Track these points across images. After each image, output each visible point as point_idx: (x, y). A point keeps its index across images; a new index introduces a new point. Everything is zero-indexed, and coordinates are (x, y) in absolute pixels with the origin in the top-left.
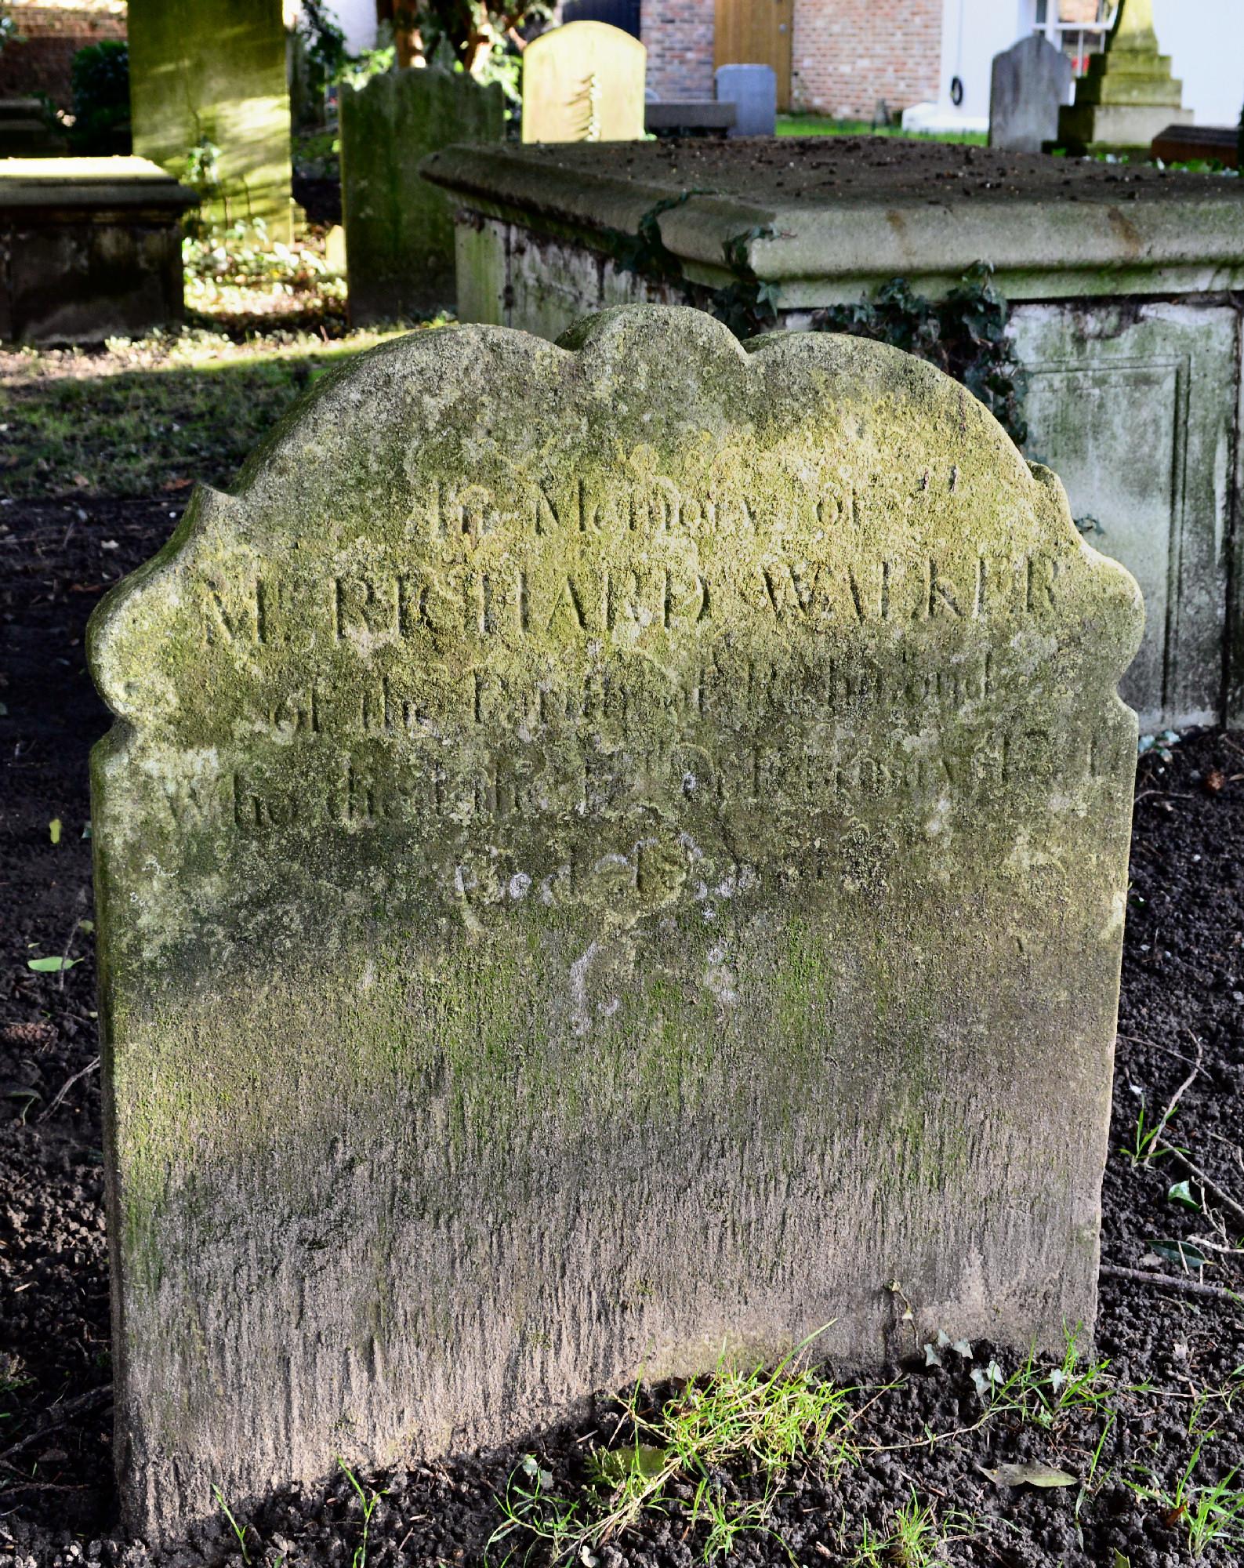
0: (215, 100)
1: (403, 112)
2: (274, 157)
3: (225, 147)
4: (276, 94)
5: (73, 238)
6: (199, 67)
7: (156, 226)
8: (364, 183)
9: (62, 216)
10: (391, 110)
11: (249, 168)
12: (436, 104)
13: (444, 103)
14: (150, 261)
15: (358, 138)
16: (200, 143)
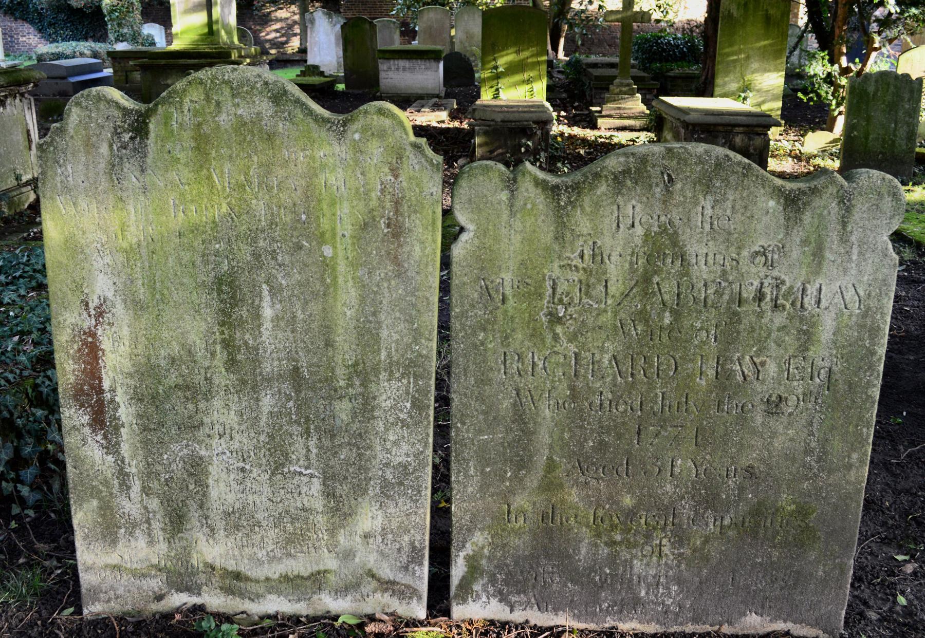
0: (753, 73)
1: (877, 90)
2: (775, 98)
3: (754, 93)
4: (780, 71)
5: (724, 138)
6: (748, 58)
7: (759, 134)
8: (855, 121)
9: (720, 128)
10: (871, 89)
11: (764, 102)
12: (892, 88)
13: (896, 87)
14: (755, 149)
15: (855, 101)
16: (744, 92)
